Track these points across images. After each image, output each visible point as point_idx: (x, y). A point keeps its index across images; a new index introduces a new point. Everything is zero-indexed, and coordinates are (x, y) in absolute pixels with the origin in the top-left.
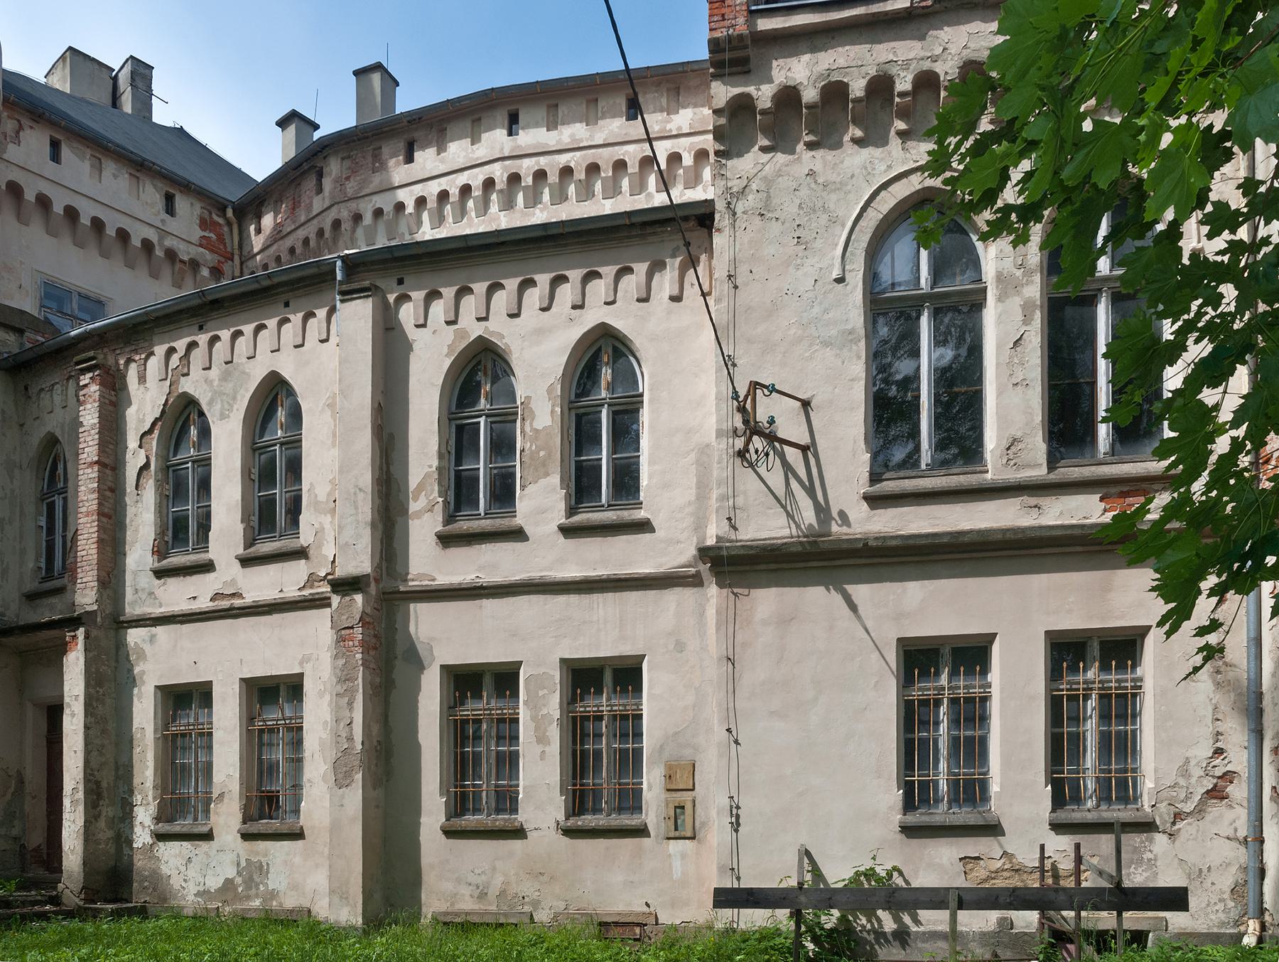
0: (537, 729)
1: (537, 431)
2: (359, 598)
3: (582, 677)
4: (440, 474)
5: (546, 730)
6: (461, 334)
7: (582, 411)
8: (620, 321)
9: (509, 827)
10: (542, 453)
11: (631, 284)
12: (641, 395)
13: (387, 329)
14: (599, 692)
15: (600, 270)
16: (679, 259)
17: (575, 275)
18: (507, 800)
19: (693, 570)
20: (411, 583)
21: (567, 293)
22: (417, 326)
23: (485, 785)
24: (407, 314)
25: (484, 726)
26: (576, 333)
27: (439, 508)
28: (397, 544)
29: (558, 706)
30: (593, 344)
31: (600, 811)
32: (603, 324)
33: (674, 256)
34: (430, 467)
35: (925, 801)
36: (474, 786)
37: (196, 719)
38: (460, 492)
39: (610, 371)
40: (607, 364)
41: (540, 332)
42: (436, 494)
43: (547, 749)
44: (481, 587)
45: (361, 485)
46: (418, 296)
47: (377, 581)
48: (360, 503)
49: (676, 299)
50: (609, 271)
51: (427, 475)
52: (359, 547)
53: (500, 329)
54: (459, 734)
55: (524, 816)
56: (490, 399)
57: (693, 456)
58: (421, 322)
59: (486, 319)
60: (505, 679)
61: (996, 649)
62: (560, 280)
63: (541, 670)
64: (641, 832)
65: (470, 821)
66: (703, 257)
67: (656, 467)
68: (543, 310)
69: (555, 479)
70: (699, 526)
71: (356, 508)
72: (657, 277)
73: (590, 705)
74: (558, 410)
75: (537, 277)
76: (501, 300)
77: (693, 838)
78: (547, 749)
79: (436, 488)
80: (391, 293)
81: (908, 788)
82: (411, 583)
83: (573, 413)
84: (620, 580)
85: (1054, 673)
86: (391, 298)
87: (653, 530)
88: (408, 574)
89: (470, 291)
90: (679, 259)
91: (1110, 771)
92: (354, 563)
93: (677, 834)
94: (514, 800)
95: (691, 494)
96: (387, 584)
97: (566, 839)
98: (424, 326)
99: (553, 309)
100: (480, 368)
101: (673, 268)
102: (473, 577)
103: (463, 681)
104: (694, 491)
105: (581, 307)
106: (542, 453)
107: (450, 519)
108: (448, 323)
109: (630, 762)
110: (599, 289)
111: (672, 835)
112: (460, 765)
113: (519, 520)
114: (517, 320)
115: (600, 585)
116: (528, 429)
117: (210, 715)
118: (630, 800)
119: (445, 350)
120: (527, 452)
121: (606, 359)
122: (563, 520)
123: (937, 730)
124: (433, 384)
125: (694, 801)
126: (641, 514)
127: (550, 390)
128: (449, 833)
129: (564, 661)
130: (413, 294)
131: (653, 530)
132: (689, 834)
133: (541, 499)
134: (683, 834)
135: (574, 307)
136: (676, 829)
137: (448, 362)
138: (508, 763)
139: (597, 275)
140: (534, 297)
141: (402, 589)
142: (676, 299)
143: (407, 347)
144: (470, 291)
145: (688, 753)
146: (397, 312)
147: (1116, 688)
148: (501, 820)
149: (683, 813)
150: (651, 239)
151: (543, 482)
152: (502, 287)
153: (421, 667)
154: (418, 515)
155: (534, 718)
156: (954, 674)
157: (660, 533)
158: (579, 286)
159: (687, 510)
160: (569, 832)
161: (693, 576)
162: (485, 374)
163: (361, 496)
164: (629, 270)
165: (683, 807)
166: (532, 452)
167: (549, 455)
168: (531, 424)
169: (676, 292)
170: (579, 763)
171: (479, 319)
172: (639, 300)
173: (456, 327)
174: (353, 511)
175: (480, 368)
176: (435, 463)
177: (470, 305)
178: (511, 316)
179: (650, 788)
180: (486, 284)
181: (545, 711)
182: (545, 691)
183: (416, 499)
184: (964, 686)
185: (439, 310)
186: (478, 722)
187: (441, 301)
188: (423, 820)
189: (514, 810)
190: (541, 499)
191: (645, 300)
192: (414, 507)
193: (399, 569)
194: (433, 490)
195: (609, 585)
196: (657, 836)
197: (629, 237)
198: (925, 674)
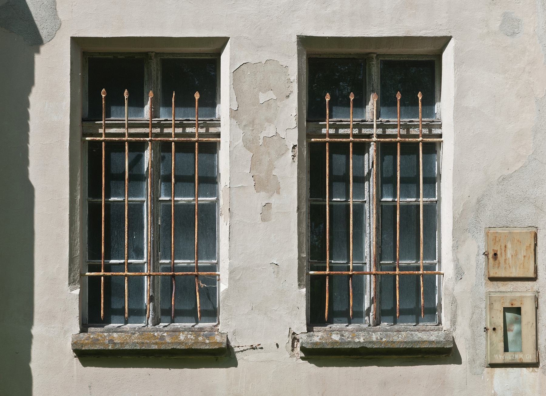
0: (255, 163)
3: (334, 72)
5: (271, 166)
9: (205, 343)
14: (137, 102)
18: (192, 295)
23: (142, 263)
25: (147, 155)
29: (294, 123)
31: (358, 315)
35: (113, 312)
36: (132, 267)
37: (155, 114)
43: (274, 200)
54: (99, 168)
55: (230, 325)
60: (189, 71)
61: (448, 58)
63: (264, 56)
64: (445, 354)
65: (120, 333)
73: (342, 124)
77: (535, 365)
78: (274, 200)
81: (316, 291)
85: (313, 111)
91: (418, 268)
93: (508, 358)
94: (210, 294)
97: (310, 367)
103: (110, 71)
109: (411, 228)
111: (500, 358)
112: (100, 230)
118: (414, 296)
123: (360, 192)
125: (536, 299)
128: (87, 356)
129: (304, 42)
132: (529, 358)
134: (519, 357)
136: (506, 349)
138: (196, 226)
145: (525, 215)
147: (378, 136)
148: (183, 333)
149: (518, 321)
153: (36, 41)
155: (248, 144)
156: (386, 102)
160: (316, 355)
165: (518, 311)
170: (324, 228)
179: (459, 274)
181: (270, 131)
182: (271, 95)
184: (398, 125)
186: (138, 148)
188: (36, 330)
189: (212, 313)
196: (472, 361)
198: (340, 102)
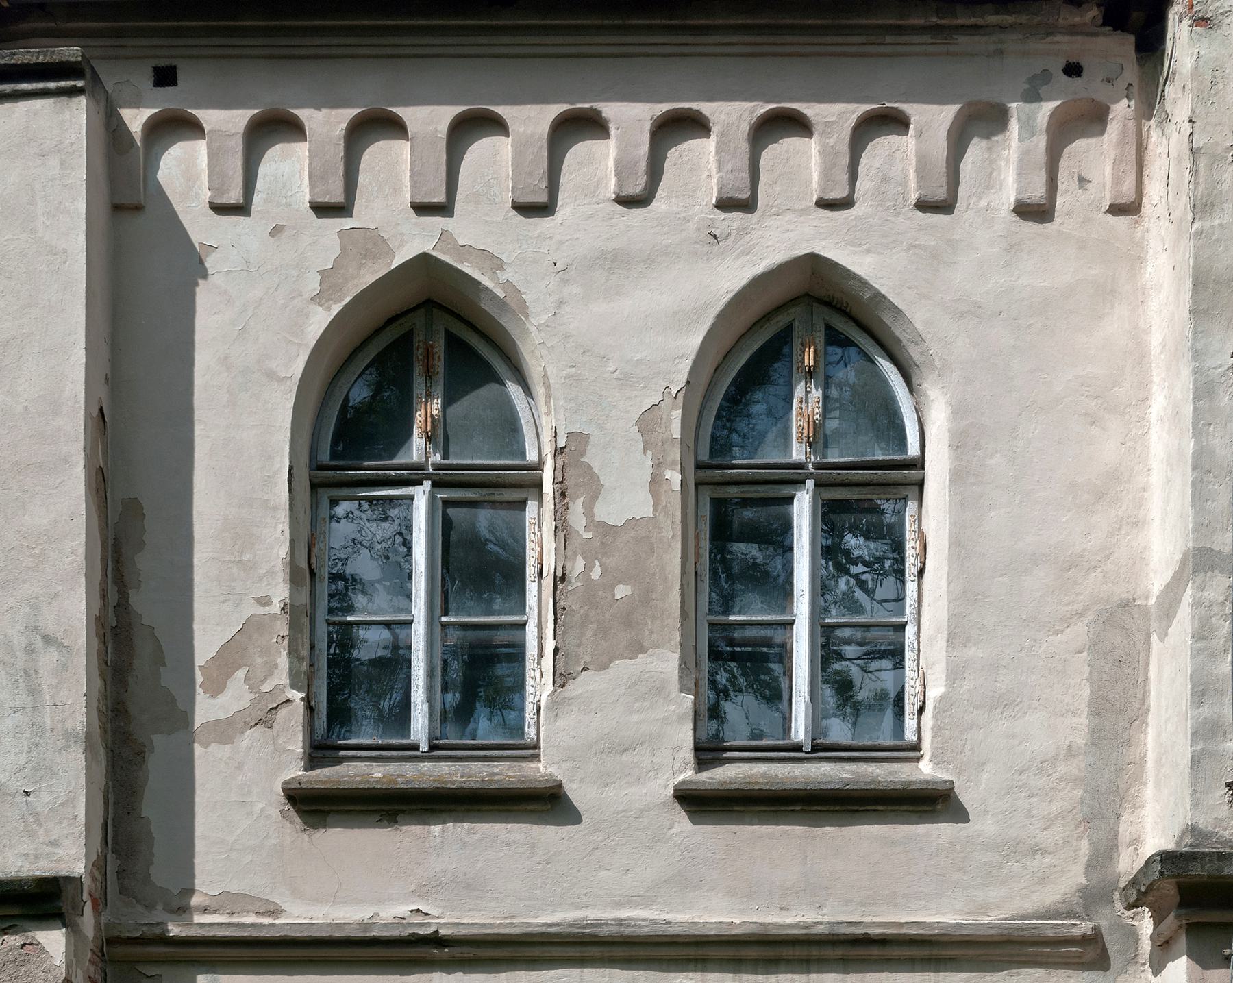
1: (605, 529)
2: (53, 942)
4: (294, 625)
6: (372, 243)
7: (733, 492)
8: (867, 253)
10: (621, 591)
11: (899, 160)
12: (918, 464)
13: (117, 208)
15: (809, 110)
16: (1047, 108)
17: (732, 116)
19: (1085, 927)
20: (198, 919)
21: (701, 165)
22: (220, 209)
24: (187, 173)
26: (731, 276)
27: (293, 716)
28: (149, 808)
30: (766, 317)
32: (814, 265)
33: (1032, 96)
34: (264, 601)
38: (346, 685)
39: (816, 394)
40: (810, 374)
41: (616, 263)
42: (282, 676)
44: (436, 940)
45: (49, 623)
46: (227, 122)
47: (99, 904)
48: (46, 679)
49: (1035, 212)
50: (835, 117)
51: (252, 626)
52: (42, 801)
53: (483, 238)
56: (439, 435)
57: (1080, 631)
58: (234, 195)
59: (443, 209)
62: (679, 126)
66: (1122, 110)
67: (972, 652)
68: (627, 202)
69: (666, 662)
70: (1104, 807)
71: (34, 691)
72: (976, 150)
74: (674, 477)
75: (610, 110)
76: (494, 163)
79: (283, 660)
80: (136, 104)
82: (198, 919)
83: (706, 495)
84: (866, 941)
86: (136, 119)
87: (959, 814)
88: (190, 891)
89: (396, 127)
90: (1047, 108)
92: (26, 846)
95: (1077, 728)
96: (135, 920)
98: (241, 209)
99: (660, 204)
100: (417, 352)
101: (1028, 129)
102: (403, 910)
104: (1083, 721)
105: (747, 205)
106: (621, 591)
107: (320, 751)
108: (322, 209)
110: (802, 162)
113: (545, 768)
114: (542, 225)
115: (799, 952)
116: (577, 519)
117: (1196, 257)
119: (313, 284)
120: (575, 583)
121: (809, 359)
122: (689, 774)
124: (271, 375)
126: (926, 770)
127: (648, 422)
130: (209, 117)
131: (959, 814)
133: (610, 711)
135: (725, 205)
137: (319, 320)
139: (798, 125)
140: (597, 165)
141: (175, 930)
142: (1035, 212)
143: (192, 265)
144: (396, 127)
146: (152, 164)
150: (963, 42)
151: (623, 668)
152: (497, 125)
154: (225, 731)
157: (982, 825)
158: (744, 147)
159: (1061, 769)
161: (1084, 940)
162: (429, 374)
163: (49, 658)
164: (896, 122)
166: (589, 583)
167: (646, 596)
168: (588, 511)
169: (1036, 192)
171: (422, 209)
172: (924, 206)
173: (347, 223)
174: (22, 699)
175: (417, 352)
176: (280, 592)
177: (393, 168)
178: (526, 209)
180: (447, 114)
183: (216, 688)
185: (290, 170)
187: (301, 149)
190: (610, 711)
191: (937, 206)
192: (207, 709)
193: (160, 875)
194: (272, 668)
195: (829, 952)
197: (899, 30)
